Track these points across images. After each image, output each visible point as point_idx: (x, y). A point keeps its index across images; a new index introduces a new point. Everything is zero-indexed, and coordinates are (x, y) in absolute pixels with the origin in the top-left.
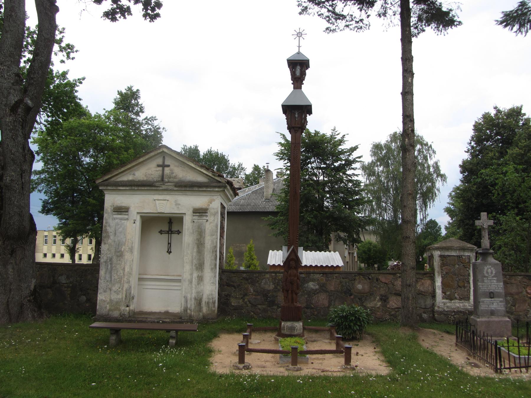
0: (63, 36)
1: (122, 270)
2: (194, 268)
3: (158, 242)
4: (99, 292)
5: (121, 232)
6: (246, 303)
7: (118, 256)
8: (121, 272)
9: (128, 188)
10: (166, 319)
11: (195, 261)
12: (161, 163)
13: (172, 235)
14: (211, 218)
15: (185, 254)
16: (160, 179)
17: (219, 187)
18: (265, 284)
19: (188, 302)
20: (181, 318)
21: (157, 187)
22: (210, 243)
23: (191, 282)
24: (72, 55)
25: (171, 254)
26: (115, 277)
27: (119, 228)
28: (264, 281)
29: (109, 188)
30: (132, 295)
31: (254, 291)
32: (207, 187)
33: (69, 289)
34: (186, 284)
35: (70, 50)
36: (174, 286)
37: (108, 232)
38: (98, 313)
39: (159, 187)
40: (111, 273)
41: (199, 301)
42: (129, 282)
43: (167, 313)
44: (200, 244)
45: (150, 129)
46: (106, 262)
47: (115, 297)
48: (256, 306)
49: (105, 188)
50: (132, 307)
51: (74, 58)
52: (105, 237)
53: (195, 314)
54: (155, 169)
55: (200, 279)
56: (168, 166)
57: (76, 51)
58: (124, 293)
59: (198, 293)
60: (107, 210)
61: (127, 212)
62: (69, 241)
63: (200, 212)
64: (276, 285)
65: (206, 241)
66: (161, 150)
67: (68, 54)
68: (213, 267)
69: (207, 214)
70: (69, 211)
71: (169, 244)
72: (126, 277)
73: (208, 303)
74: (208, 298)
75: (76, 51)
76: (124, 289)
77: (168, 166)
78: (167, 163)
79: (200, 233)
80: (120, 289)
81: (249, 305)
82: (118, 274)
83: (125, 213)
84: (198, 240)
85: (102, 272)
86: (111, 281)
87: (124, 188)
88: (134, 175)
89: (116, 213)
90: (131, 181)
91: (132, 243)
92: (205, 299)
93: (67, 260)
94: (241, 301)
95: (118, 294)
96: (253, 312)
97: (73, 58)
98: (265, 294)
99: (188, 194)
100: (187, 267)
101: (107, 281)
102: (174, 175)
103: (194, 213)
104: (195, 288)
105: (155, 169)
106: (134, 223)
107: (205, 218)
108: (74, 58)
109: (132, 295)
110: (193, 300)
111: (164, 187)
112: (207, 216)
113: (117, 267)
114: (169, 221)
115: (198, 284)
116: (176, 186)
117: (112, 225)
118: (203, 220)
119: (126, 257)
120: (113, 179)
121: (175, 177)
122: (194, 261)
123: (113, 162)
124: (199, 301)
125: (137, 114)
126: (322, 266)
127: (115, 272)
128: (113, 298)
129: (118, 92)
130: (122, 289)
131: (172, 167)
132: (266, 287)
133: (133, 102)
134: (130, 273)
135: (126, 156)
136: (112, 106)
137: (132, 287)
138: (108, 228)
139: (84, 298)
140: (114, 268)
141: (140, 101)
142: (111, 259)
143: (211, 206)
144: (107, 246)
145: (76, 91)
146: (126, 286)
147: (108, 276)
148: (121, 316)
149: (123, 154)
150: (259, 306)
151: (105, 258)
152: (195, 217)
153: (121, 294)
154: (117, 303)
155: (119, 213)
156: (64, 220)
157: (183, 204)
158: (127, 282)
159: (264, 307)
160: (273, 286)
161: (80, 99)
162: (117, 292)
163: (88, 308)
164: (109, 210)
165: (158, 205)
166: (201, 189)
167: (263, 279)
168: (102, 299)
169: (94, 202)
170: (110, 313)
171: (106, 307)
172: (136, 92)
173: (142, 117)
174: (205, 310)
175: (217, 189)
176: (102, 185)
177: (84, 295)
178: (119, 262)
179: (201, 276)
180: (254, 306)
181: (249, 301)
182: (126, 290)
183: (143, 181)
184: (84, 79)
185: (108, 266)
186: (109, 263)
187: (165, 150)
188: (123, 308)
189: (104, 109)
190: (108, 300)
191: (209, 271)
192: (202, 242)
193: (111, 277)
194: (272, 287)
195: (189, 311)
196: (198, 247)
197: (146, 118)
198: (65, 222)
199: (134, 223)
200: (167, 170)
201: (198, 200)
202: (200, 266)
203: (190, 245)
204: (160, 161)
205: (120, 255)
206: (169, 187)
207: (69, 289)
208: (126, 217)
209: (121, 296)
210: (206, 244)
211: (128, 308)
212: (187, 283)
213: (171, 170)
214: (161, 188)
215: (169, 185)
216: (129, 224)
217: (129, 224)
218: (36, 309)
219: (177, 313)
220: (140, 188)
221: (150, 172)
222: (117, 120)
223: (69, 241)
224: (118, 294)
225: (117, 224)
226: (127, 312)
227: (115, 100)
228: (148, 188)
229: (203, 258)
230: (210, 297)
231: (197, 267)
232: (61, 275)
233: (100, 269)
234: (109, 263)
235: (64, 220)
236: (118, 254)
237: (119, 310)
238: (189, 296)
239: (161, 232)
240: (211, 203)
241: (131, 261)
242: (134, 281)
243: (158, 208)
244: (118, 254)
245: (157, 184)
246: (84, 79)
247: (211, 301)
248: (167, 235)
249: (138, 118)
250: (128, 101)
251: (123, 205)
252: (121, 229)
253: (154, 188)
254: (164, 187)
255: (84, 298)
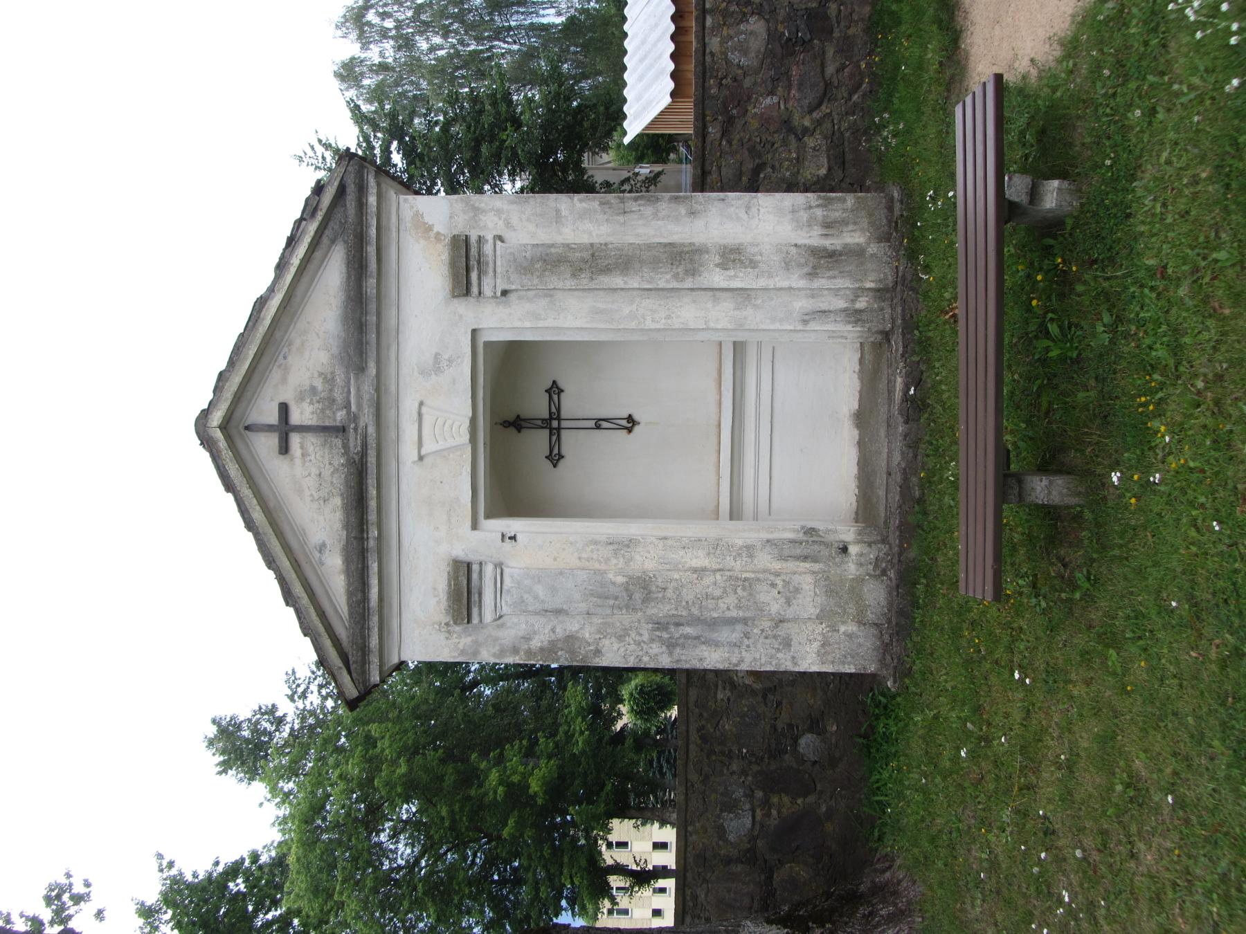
0: (22, 915)
1: (700, 578)
2: (688, 283)
3: (592, 460)
4: (788, 666)
5: (553, 590)
6: (819, 123)
7: (646, 600)
8: (709, 580)
9: (374, 567)
10: (890, 392)
11: (664, 280)
12: (273, 440)
13: (563, 415)
14: (490, 225)
15: (633, 325)
16: (338, 442)
17: (362, 189)
18: (745, 52)
19: (824, 306)
20: (886, 335)
21: (365, 445)
22: (588, 226)
23: (744, 295)
24: (79, 888)
25: (636, 417)
26: (728, 606)
27: (536, 597)
28: (734, 57)
29: (374, 642)
30: (801, 536)
31: (772, 93)
32: (360, 240)
33: (775, 800)
34: (756, 318)
35: (66, 897)
36: (758, 395)
37: (552, 642)
38: (872, 668)
39: (365, 436)
40: (713, 624)
41: (823, 260)
42: (749, 550)
43: (861, 419)
44: (593, 264)
45: (321, 687)
46: (671, 645)
47: (809, 603)
48: (828, 85)
49: (375, 659)
50: (848, 533)
51: (86, 881)
52: (572, 652)
53: (873, 276)
54: (298, 461)
55: (732, 256)
56: (284, 409)
57: (68, 876)
58: (791, 565)
59: (787, 265)
60: (463, 652)
61: (469, 565)
62: (615, 881)
63: (466, 266)
64: (748, 10)
65: (585, 239)
66: (218, 435)
67: (78, 899)
68: (683, 210)
69: (473, 240)
70: (537, 890)
71: (598, 427)
72: (729, 562)
73: (828, 225)
74: (810, 224)
75: (68, 876)
76: (777, 566)
77: (284, 409)
78: (273, 418)
79: (550, 263)
80: (779, 582)
81: (825, 109)
82: (718, 593)
83: (475, 576)
84: (576, 272)
85: (712, 658)
86: (745, 621)
87: (374, 582)
88: (322, 548)
89: (475, 611)
90: (347, 561)
91: (596, 543)
92: (814, 238)
93: (670, 884)
94: (810, 142)
95: (797, 590)
96: (850, 95)
97: (87, 885)
98: (783, 50)
99: (393, 322)
100: (688, 313)
101: (747, 635)
102: (319, 384)
103: (468, 292)
104: (770, 276)
105: (298, 461)
106: (513, 538)
107: (488, 249)
108: (86, 881)
109: (801, 536)
110: (817, 283)
111: (367, 418)
112: (480, 240)
113: (690, 597)
114: (512, 430)
115: (753, 264)
116: (362, 369)
117: (522, 629)
118: (499, 257)
119: (650, 565)
120: (342, 633)
121: (329, 380)
122: (662, 284)
123: (404, 775)
124: (823, 260)
125: (280, 721)
126: (673, 56)
127: (710, 603)
128: (813, 611)
129: (220, 773)
130: (777, 574)
131: (287, 395)
132: (757, 44)
133: (246, 733)
134: (716, 546)
135: (387, 743)
136: (259, 789)
137: (770, 536)
138: (536, 643)
139: (807, 743)
140: (695, 611)
141: (244, 714)
142: (660, 625)
143: (439, 228)
144: (606, 642)
145: (195, 875)
146: (765, 560)
147: (725, 635)
148: (884, 573)
149: (383, 750)
150: (830, 69)
151: (655, 648)
152: (487, 291)
153: (796, 578)
154: (830, 592)
155: (475, 597)
156: (564, 903)
157: (434, 338)
158: (751, 556)
159: (830, 52)
160: (752, 20)
161: (217, 863)
162: (791, 594)
163: (849, 710)
164: (466, 641)
165: (442, 445)
166: (373, 266)
167: (728, 61)
168: (818, 653)
169: (511, 822)
170: (870, 616)
171: (850, 636)
172: (219, 725)
173: (287, 709)
174: (854, 237)
175: (372, 200)
176: (364, 672)
177: (795, 741)
178: (669, 593)
179: (723, 256)
180: (827, 93)
181: (810, 112)
182: (782, 558)
183: (346, 509)
184: (160, 856)
185: (687, 637)
186: (677, 632)
187: (217, 418)
188: (851, 569)
189: (261, 804)
190: (820, 628)
191: (699, 223)
192: (586, 255)
193: (731, 622)
194: (756, 25)
195: (861, 304)
196: (607, 270)
197: (291, 698)
198: (567, 898)
199: (513, 538)
200: (301, 414)
201: (419, 273)
202: (683, 258)
203: (601, 306)
204: (265, 445)
205: (642, 589)
206: (366, 397)
207: (775, 800)
208: (489, 570)
209: (805, 577)
210: (596, 240)
211: (853, 550)
212: (749, 312)
213: (301, 398)
214: (371, 430)
215: (359, 397)
216: (519, 561)
217: (519, 561)
218: (862, 910)
219: (861, 379)
220: (372, 517)
221: (310, 483)
222: (292, 771)
223: (615, 881)
224: (797, 590)
225: (521, 607)
226: (866, 550)
227: (241, 780)
228: (371, 481)
229: (649, 247)
230: (804, 216)
231: (687, 272)
232: (721, 832)
233: (698, 666)
234: (677, 632)
235: (564, 903)
236: (638, 596)
237: (859, 580)
238: (801, 304)
239: (555, 458)
240: (430, 228)
241: (668, 549)
242: (741, 534)
243: (451, 442)
244: (638, 596)
245: (354, 444)
246: (160, 856)
247: (819, 212)
248: (564, 433)
249: (289, 719)
250: (242, 748)
251: (442, 584)
252: (540, 590)
253: (372, 459)
254: (367, 418)
255: (807, 743)
